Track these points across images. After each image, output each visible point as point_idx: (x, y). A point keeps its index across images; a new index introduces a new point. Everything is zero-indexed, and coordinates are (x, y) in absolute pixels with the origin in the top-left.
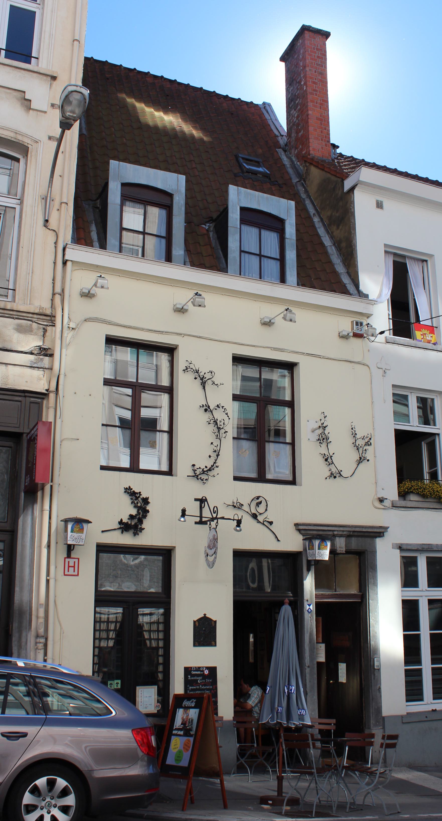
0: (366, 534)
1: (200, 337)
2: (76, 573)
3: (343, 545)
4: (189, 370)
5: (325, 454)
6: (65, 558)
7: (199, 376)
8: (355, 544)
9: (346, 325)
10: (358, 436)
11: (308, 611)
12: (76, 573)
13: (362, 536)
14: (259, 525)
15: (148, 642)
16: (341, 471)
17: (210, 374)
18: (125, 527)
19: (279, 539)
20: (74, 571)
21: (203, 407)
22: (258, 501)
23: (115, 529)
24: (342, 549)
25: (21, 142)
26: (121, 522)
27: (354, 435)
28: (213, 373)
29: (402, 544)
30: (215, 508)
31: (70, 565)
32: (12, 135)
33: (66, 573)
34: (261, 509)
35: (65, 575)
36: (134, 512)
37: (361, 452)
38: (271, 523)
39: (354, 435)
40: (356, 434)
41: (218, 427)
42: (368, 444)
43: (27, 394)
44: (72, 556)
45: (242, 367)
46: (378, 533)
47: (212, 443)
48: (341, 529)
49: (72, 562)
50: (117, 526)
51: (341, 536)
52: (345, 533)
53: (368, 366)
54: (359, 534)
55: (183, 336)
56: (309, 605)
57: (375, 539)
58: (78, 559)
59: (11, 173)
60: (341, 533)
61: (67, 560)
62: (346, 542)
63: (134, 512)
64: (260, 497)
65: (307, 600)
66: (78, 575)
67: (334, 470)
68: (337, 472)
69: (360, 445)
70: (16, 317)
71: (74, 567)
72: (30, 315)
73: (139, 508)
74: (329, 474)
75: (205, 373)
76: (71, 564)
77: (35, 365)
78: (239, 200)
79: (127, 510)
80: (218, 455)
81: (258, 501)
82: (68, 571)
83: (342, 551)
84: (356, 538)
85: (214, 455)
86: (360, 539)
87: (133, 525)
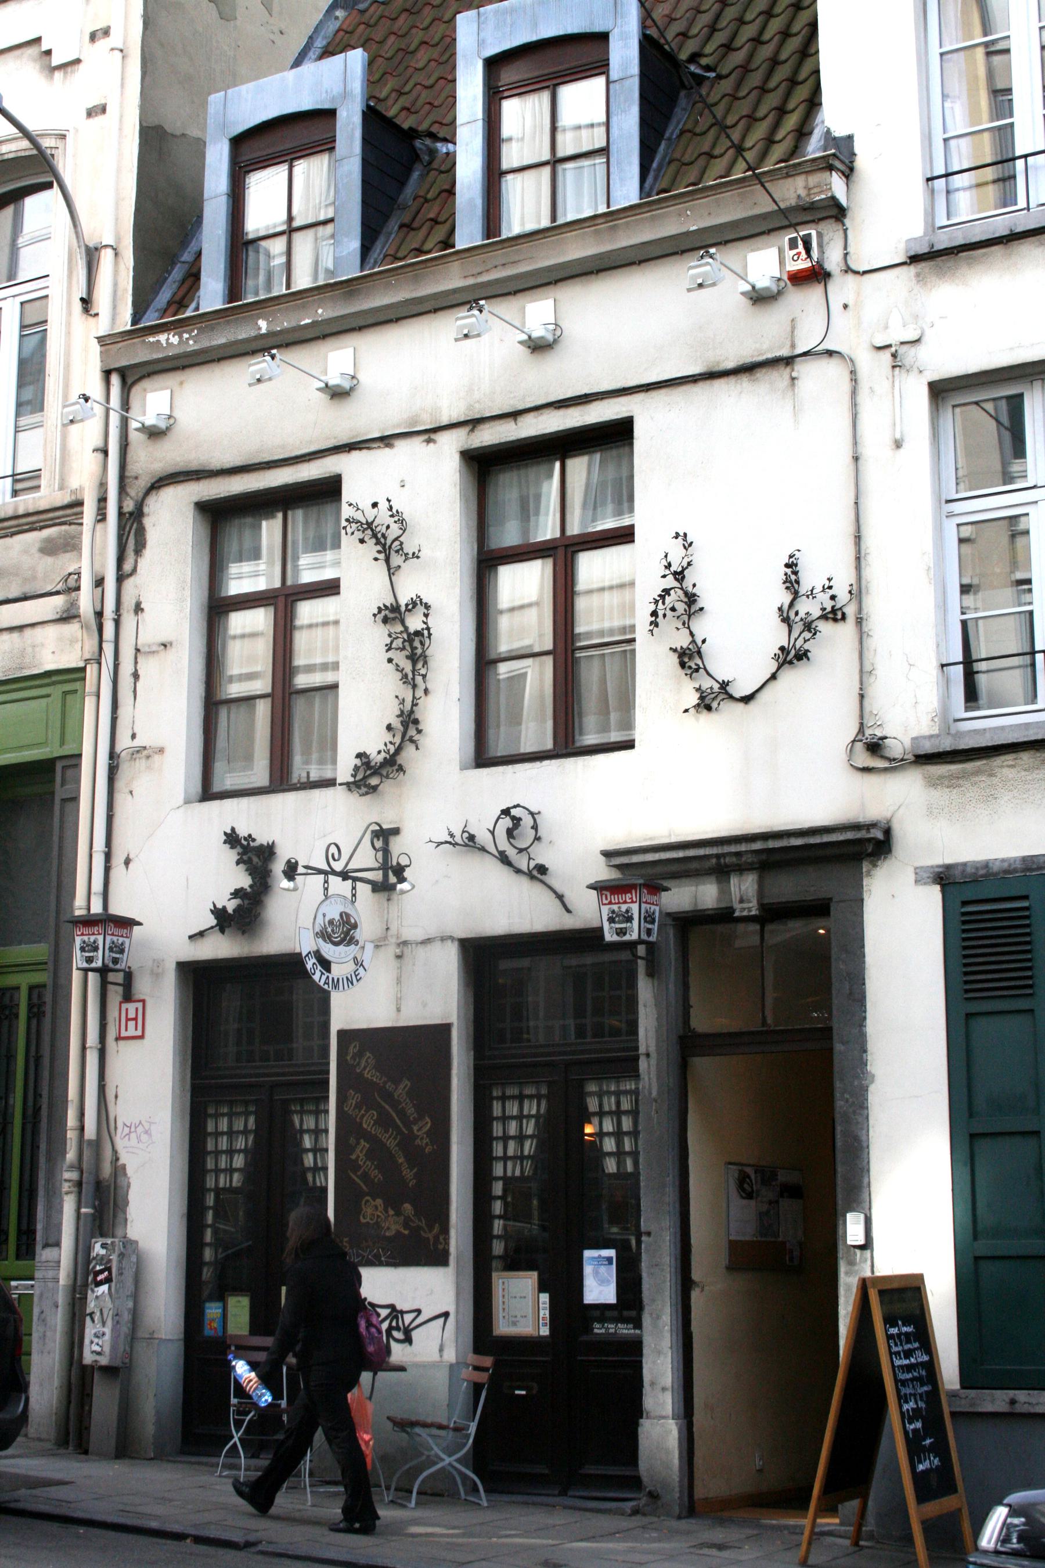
6: (121, 1003)
8: (788, 887)
9: (826, 567)
12: (139, 1033)
18: (223, 919)
22: (512, 819)
24: (745, 905)
26: (219, 913)
29: (948, 867)
31: (134, 1022)
36: (244, 881)
43: (54, 678)
45: (581, 734)
46: (864, 846)
49: (131, 1007)
50: (212, 921)
59: (251, 624)
61: (124, 1006)
63: (244, 881)
66: (142, 1037)
71: (136, 1019)
73: (252, 871)
74: (694, 699)
78: (481, 43)
79: (228, 879)
81: (512, 819)
87: (243, 914)
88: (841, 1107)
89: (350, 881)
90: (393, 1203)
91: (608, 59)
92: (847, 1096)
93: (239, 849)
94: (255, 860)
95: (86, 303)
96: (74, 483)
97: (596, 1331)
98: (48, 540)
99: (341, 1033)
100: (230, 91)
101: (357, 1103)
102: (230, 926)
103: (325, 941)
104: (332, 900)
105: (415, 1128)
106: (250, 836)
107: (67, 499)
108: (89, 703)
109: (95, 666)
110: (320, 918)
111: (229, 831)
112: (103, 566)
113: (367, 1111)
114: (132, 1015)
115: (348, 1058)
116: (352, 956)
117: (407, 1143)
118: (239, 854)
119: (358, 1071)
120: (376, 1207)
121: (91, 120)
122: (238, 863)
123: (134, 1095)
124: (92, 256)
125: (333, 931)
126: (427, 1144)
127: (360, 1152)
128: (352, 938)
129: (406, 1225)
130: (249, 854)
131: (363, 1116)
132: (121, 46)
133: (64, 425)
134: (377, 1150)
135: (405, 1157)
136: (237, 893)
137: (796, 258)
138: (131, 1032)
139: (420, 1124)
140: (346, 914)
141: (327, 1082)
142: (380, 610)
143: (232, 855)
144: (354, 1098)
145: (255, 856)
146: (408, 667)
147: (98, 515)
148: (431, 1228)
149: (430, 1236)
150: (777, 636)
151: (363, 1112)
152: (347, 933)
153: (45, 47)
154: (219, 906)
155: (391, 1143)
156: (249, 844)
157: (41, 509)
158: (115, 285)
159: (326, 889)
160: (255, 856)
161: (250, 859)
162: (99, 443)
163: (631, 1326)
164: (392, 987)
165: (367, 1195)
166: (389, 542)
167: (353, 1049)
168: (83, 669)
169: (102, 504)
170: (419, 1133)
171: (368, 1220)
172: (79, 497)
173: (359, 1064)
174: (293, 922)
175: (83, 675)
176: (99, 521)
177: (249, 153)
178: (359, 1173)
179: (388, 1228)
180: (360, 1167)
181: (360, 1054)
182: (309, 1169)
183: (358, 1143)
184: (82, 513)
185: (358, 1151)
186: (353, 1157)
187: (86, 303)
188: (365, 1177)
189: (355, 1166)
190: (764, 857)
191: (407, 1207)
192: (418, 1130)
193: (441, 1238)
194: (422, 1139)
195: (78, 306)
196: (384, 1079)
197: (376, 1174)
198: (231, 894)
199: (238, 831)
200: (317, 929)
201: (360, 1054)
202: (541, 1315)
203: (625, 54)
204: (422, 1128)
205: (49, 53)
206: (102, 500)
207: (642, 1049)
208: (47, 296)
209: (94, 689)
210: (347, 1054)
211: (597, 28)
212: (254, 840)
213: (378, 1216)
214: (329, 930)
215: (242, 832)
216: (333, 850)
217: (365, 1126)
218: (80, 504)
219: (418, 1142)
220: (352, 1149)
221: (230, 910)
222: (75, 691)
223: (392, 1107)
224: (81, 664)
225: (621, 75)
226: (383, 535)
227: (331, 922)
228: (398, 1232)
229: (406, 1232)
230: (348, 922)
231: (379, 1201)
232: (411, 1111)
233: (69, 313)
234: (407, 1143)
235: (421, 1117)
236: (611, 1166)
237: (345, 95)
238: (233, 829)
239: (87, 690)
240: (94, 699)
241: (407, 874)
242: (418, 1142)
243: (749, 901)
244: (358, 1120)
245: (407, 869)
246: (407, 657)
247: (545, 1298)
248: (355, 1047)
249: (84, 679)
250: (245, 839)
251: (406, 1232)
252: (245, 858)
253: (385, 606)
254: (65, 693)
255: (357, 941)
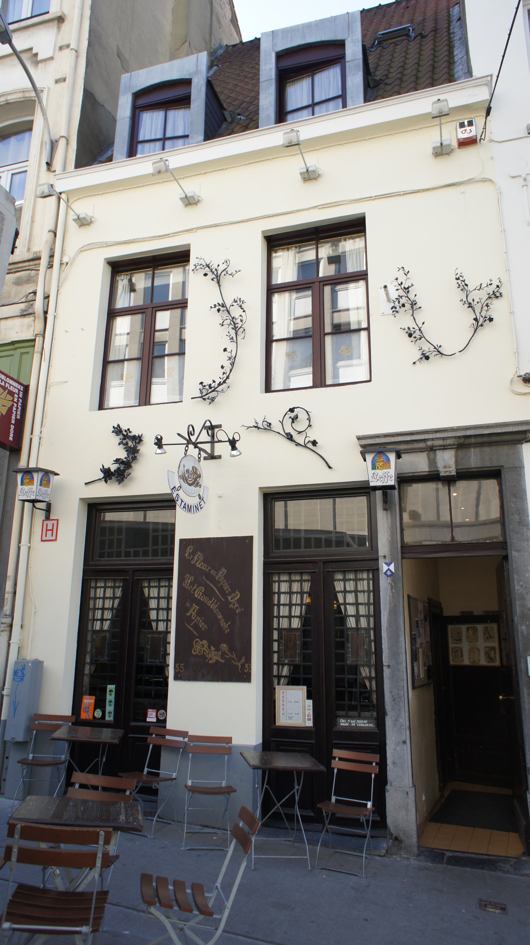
0: (495, 439)
1: (216, 226)
2: (54, 538)
3: (451, 462)
4: (198, 267)
5: (409, 328)
6: (44, 521)
7: (211, 271)
10: (471, 288)
11: (385, 573)
12: (54, 538)
13: (490, 444)
14: (299, 448)
15: (154, 624)
16: (440, 346)
17: (225, 264)
19: (331, 466)
20: (52, 536)
21: (215, 307)
23: (100, 479)
24: (448, 469)
25: (29, 99)
27: (463, 285)
28: (228, 262)
30: (191, 427)
32: (20, 95)
33: (44, 538)
34: (301, 425)
35: (42, 541)
36: (123, 455)
37: (478, 311)
38: (314, 443)
39: (463, 285)
40: (467, 285)
41: (236, 328)
42: (496, 295)
43: (17, 345)
44: (51, 518)
47: (225, 350)
48: (439, 435)
49: (50, 523)
50: (102, 475)
51: (444, 448)
52: (449, 442)
53: (490, 181)
54: (479, 440)
55: (195, 230)
56: (388, 564)
57: (519, 446)
58: (58, 520)
60: (441, 442)
61: (45, 522)
62: (456, 457)
63: (123, 455)
64: (294, 408)
65: (385, 557)
66: (56, 539)
67: (426, 347)
68: (432, 348)
69: (477, 300)
70: (16, 270)
71: (52, 530)
72: (27, 264)
75: (218, 266)
76: (50, 527)
77: (25, 313)
78: (274, 45)
80: (233, 364)
82: (46, 536)
83: (450, 472)
84: (478, 450)
85: (227, 365)
86: (487, 449)
87: (119, 473)
88: (518, 590)
89: (197, 450)
90: (214, 643)
91: (345, 54)
92: (521, 583)
93: (121, 436)
94: (130, 444)
95: (49, 164)
96: (36, 248)
97: (342, 724)
98: (19, 278)
99: (181, 541)
100: (133, 73)
101: (191, 582)
102: (111, 479)
103: (184, 482)
104: (189, 458)
105: (229, 598)
106: (129, 429)
107: (31, 256)
108: (36, 357)
109: (41, 338)
110: (182, 466)
111: (116, 426)
112: (49, 290)
113: (197, 587)
114: (50, 527)
115: (186, 555)
116: (198, 494)
117: (224, 607)
118: (120, 439)
119: (192, 563)
120: (203, 645)
121: (57, 85)
122: (119, 444)
123: (52, 570)
124: (53, 145)
125: (188, 476)
126: (237, 608)
127: (193, 611)
128: (198, 483)
129: (222, 657)
130: (127, 440)
131: (194, 591)
132: (76, 49)
133: (37, 197)
134: (203, 610)
135: (222, 614)
136: (117, 461)
137: (464, 132)
138: (49, 537)
139: (233, 595)
140: (195, 468)
141: (172, 570)
142: (215, 306)
143: (117, 439)
144: (189, 579)
145: (131, 442)
146: (233, 333)
147: (49, 265)
148: (239, 660)
149: (239, 664)
150: (468, 317)
151: (195, 587)
152: (196, 480)
153: (34, 51)
154: (106, 467)
155: (213, 607)
156: (127, 434)
157: (16, 261)
158: (66, 157)
159: (186, 451)
160: (131, 442)
161: (127, 444)
162: (52, 228)
163: (366, 721)
164: (222, 510)
165: (197, 637)
166: (219, 273)
167: (189, 550)
168: (34, 340)
169: (52, 259)
170: (231, 601)
171: (197, 653)
172: (38, 255)
173: (192, 559)
174: (151, 477)
175: (33, 343)
176: (49, 268)
177: (142, 102)
178: (192, 624)
179: (211, 658)
180: (193, 620)
181: (193, 553)
182: (154, 621)
183: (192, 606)
184: (39, 264)
185: (191, 611)
186: (188, 614)
187: (49, 164)
188: (196, 627)
189: (189, 620)
190: (462, 441)
191: (224, 646)
192: (231, 599)
193: (246, 666)
194: (234, 604)
195: (44, 166)
196: (209, 568)
197: (203, 625)
198: (114, 461)
199: (121, 426)
200: (180, 474)
201: (193, 553)
202: (307, 714)
203: (353, 51)
204: (234, 598)
205: (36, 55)
206: (52, 256)
207: (381, 553)
208: (26, 171)
209: (40, 350)
210: (185, 553)
211: (339, 37)
212: (130, 432)
213: (204, 651)
214: (187, 475)
215: (124, 427)
216: (191, 429)
217: (196, 596)
218: (39, 259)
219: (231, 606)
220: (188, 610)
221: (112, 470)
222: (28, 353)
223: (214, 585)
224: (34, 338)
225: (352, 58)
226: (216, 270)
227: (188, 471)
228: (217, 661)
229: (223, 661)
230: (196, 473)
231: (205, 642)
232: (226, 587)
233: (39, 171)
234: (224, 607)
235: (233, 591)
236: (351, 623)
237: (197, 72)
238: (118, 426)
239: (35, 350)
240: (39, 355)
241: (237, 445)
242: (231, 606)
243: (450, 467)
244: (192, 592)
245: (237, 443)
246: (233, 328)
247: (310, 702)
248: (190, 549)
249: (34, 346)
250: (126, 431)
251: (223, 661)
252: (124, 442)
253: (218, 304)
254: (22, 354)
255: (200, 485)
